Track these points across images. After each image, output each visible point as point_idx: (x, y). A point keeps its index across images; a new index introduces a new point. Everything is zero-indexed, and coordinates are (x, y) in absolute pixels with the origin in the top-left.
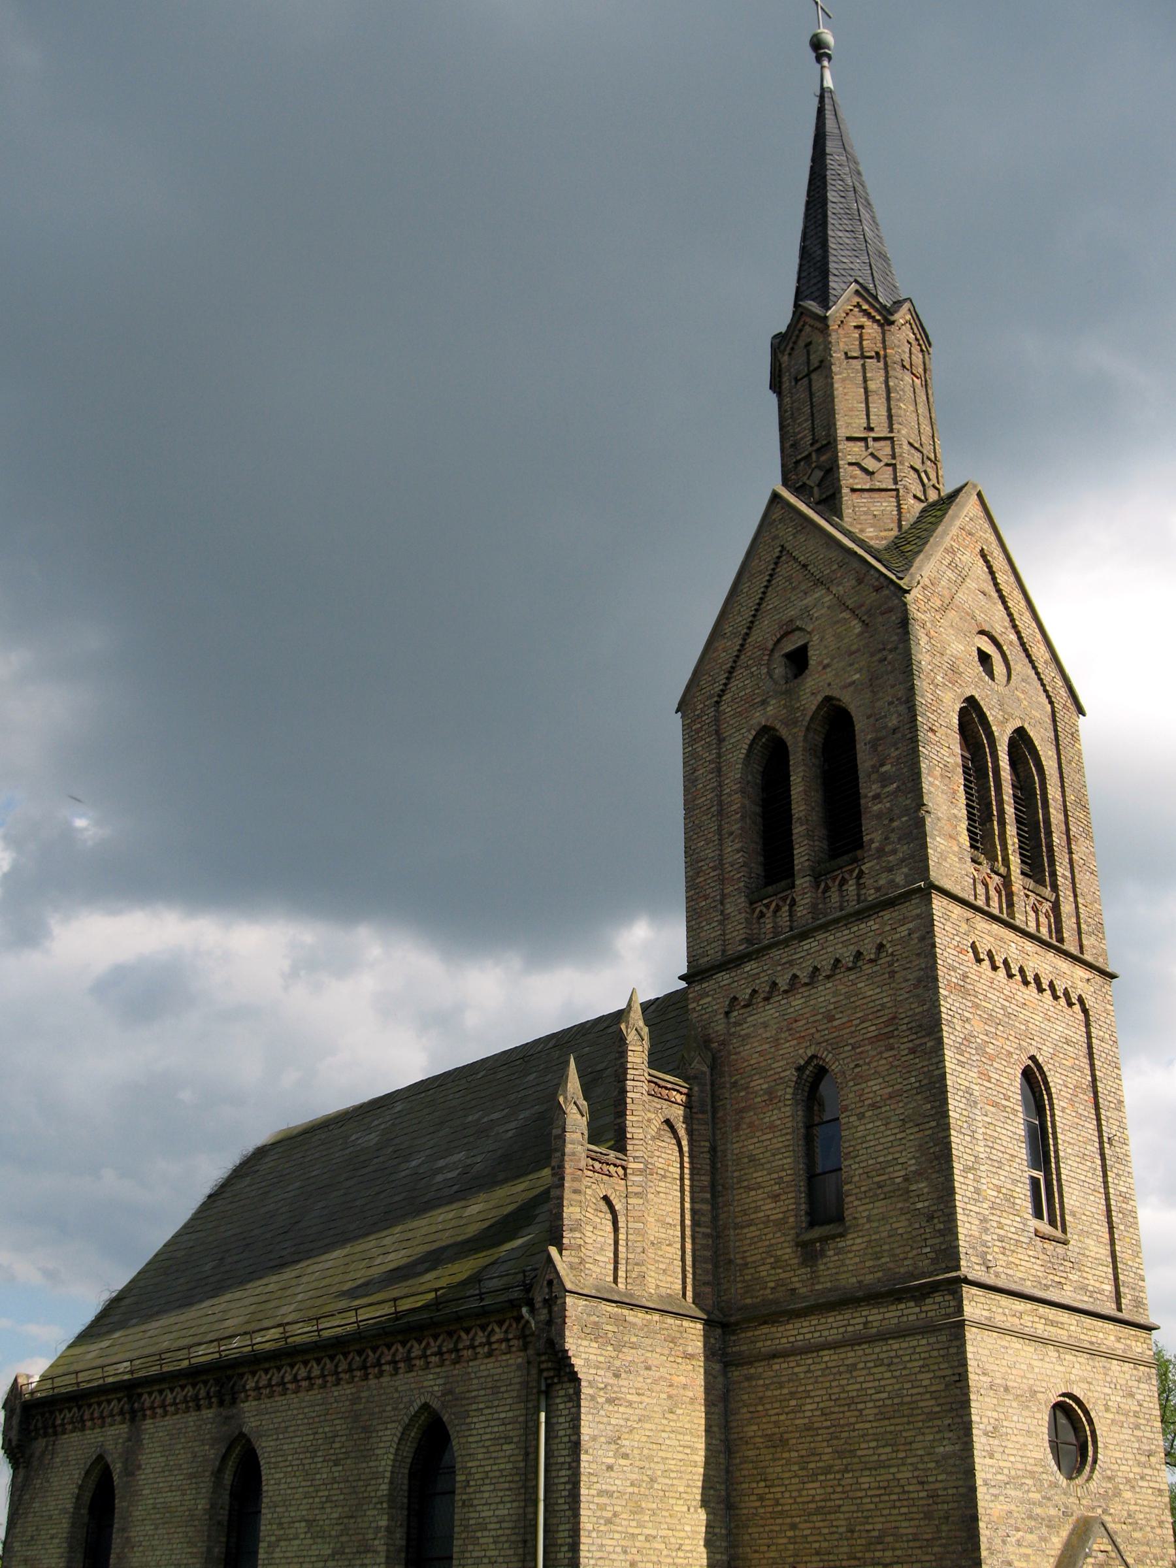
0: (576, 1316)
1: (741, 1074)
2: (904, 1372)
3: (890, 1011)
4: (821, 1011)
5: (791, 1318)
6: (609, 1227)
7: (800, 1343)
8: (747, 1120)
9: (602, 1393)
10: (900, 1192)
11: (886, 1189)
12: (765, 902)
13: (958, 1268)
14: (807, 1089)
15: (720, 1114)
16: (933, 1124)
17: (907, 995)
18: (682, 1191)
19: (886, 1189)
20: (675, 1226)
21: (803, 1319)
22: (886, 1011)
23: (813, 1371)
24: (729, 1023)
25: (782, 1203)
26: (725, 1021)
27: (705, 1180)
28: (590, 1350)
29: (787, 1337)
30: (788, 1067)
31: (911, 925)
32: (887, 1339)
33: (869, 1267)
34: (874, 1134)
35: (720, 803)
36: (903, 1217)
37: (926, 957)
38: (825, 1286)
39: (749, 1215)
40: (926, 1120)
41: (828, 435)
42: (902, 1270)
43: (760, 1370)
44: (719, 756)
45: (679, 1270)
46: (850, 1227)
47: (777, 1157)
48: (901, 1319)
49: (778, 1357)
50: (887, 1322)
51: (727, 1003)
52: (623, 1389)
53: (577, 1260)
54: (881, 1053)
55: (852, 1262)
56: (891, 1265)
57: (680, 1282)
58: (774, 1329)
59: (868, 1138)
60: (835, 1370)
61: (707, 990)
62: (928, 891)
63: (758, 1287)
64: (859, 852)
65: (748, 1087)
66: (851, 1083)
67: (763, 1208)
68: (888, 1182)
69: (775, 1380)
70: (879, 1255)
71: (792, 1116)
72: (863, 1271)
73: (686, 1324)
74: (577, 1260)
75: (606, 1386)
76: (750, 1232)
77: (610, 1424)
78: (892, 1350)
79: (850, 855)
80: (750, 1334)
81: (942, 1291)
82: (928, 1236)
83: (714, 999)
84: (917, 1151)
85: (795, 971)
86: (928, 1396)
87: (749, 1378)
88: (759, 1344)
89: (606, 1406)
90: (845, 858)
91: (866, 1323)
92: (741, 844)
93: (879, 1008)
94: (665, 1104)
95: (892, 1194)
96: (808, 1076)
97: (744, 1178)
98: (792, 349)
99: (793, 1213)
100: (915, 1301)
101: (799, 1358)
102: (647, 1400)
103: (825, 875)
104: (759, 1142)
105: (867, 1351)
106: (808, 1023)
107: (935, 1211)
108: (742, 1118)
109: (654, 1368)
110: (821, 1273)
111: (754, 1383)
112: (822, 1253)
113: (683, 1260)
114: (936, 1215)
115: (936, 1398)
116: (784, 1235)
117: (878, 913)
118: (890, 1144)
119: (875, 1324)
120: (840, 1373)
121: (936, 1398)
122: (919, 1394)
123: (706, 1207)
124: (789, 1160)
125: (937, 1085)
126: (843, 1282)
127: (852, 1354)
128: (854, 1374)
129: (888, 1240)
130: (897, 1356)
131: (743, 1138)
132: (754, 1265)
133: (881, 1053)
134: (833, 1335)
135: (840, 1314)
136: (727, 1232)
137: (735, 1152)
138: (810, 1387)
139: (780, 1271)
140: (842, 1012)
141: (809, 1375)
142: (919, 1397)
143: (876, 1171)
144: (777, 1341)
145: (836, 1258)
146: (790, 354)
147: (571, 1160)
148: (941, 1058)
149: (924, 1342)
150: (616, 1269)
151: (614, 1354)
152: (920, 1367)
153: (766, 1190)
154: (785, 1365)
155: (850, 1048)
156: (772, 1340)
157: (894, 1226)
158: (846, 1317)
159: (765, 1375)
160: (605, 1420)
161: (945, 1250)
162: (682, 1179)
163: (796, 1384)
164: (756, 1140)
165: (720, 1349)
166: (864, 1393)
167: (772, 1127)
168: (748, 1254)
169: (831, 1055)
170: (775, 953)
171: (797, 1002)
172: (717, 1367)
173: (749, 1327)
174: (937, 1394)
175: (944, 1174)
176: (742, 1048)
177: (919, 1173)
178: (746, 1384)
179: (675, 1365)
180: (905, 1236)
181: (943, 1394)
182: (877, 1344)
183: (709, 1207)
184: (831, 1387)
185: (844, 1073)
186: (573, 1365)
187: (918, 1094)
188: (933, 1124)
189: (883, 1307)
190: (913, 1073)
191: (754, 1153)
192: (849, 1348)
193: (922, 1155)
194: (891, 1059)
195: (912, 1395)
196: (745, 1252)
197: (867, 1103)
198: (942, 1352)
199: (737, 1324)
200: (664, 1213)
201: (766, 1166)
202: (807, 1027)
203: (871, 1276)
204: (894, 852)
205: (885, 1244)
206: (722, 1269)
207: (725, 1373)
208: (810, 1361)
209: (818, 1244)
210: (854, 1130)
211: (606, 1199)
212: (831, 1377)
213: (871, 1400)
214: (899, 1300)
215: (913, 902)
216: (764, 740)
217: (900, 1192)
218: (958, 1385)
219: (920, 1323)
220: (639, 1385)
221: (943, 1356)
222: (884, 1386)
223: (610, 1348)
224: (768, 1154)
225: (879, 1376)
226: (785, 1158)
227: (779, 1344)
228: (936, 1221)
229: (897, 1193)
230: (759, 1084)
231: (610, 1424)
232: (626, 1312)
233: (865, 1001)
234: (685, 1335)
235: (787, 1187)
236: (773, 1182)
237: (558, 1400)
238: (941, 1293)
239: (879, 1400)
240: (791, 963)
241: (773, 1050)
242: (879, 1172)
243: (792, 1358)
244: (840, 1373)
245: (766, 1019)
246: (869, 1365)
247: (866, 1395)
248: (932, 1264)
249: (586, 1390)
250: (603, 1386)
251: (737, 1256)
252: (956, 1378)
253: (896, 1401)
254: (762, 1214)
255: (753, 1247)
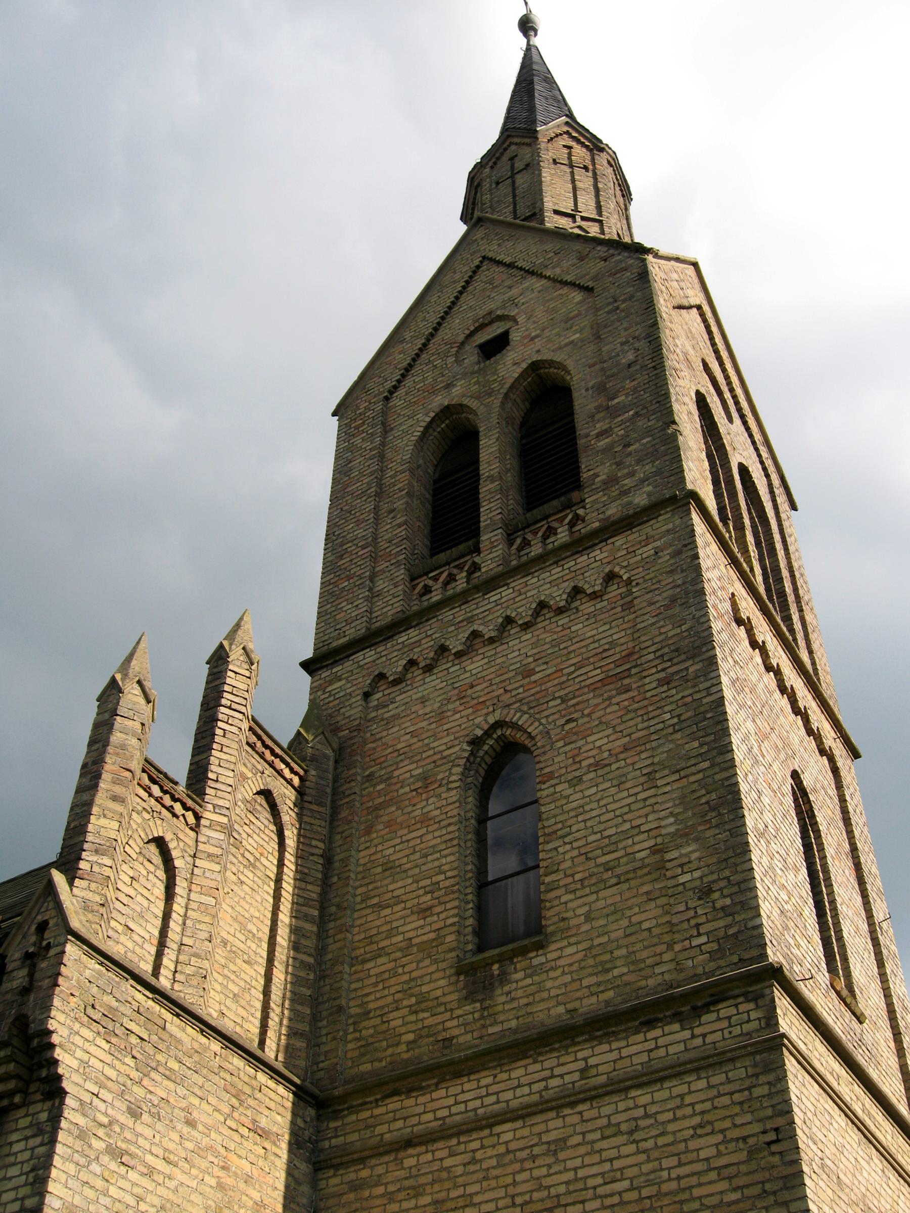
0: (78, 981)
1: (380, 764)
2: (661, 1141)
3: (624, 647)
4: (512, 668)
5: (444, 1080)
6: (159, 890)
7: (458, 1118)
8: (385, 819)
9: (101, 1132)
10: (646, 871)
11: (618, 871)
12: (431, 575)
13: (765, 956)
14: (482, 773)
15: (344, 814)
16: (706, 764)
17: (653, 620)
18: (277, 896)
19: (618, 871)
20: (260, 940)
21: (465, 1079)
22: (618, 649)
23: (481, 1161)
24: (367, 708)
25: (435, 918)
26: (363, 703)
27: (314, 891)
28: (93, 1049)
29: (434, 1111)
30: (457, 742)
31: (658, 543)
32: (627, 1089)
33: (588, 987)
34: (598, 801)
35: (380, 485)
36: (652, 904)
37: (683, 571)
38: (506, 1026)
39: (377, 942)
40: (692, 762)
41: (533, 205)
42: (651, 982)
43: (380, 1170)
44: (383, 444)
45: (259, 1005)
46: (553, 934)
47: (430, 858)
48: (653, 1055)
49: (415, 1145)
50: (627, 1062)
51: (369, 681)
52: (141, 1141)
53: (97, 898)
54: (610, 698)
55: (557, 983)
56: (631, 978)
57: (257, 1023)
58: (411, 1102)
59: (587, 808)
60: (524, 1154)
61: (339, 674)
62: (684, 502)
63: (385, 1043)
64: (575, 496)
65: (389, 778)
66: (561, 744)
67: (401, 929)
68: (624, 860)
69: (407, 1183)
70: (608, 966)
71: (459, 801)
72: (579, 994)
73: (262, 1077)
74: (97, 898)
75: (111, 1123)
76: (383, 964)
77: (106, 1193)
78: (637, 1107)
79: (562, 499)
80: (365, 1114)
81: (735, 997)
82: (703, 919)
83: (348, 682)
84: (675, 806)
85: (475, 627)
86: (713, 1175)
87: (355, 1187)
88: (379, 1130)
89: (105, 1159)
90: (555, 503)
91: (583, 1071)
92: (404, 518)
93: (606, 647)
94: (269, 771)
95: (631, 875)
96: (486, 753)
97: (373, 893)
98: (495, 163)
99: (454, 929)
100: (681, 1022)
101: (454, 1141)
102: (181, 1177)
103: (523, 529)
104: (402, 842)
105: (587, 1115)
106: (491, 685)
107: (714, 881)
108: (377, 817)
109: (200, 1127)
110: (500, 1008)
111: (366, 1193)
112: (503, 978)
113: (267, 992)
114: (715, 887)
115: (730, 1178)
116: (436, 962)
117: (606, 540)
118: (626, 809)
119: (601, 1069)
120: (534, 1158)
121: (730, 1178)
122: (693, 1174)
123: (312, 928)
124: (451, 858)
125: (709, 715)
126: (542, 1016)
127: (559, 1122)
128: (562, 1155)
129: (624, 942)
130: (646, 1116)
131: (376, 842)
132: (378, 1013)
133: (610, 698)
134: (524, 1096)
135: (535, 1062)
136: (339, 968)
137: (362, 861)
138: (470, 1189)
139: (426, 1015)
140: (547, 663)
141: (472, 1168)
142: (694, 1180)
143: (602, 848)
144: (415, 1120)
145: (529, 981)
146: (492, 167)
147: (117, 754)
148: (715, 681)
149: (702, 1084)
150: (159, 955)
151: (135, 1075)
152: (694, 1128)
153: (409, 904)
154: (429, 1157)
155: (559, 701)
156: (405, 1118)
157: (634, 919)
158: (547, 1064)
159: (390, 1177)
160: (99, 1183)
161: (735, 935)
162: (278, 880)
163: (447, 1185)
164: (398, 841)
165: (309, 1141)
166: (580, 1185)
167: (425, 820)
168: (372, 997)
169: (527, 716)
170: (447, 615)
171: (475, 665)
172: (304, 1167)
173: (365, 1103)
174: (732, 1170)
175: (727, 827)
176: (385, 733)
177: (683, 835)
178: (352, 1196)
179: (236, 1137)
180: (655, 931)
181: (743, 1168)
182: (607, 1099)
183: (315, 929)
184: (515, 1183)
185: (548, 733)
186: (56, 1062)
187: (675, 732)
188: (706, 764)
189: (618, 1040)
190: (667, 709)
191: (392, 858)
192: (553, 1114)
193: (686, 810)
194: (626, 703)
195: (679, 1178)
196: (367, 995)
197: (584, 763)
198: (737, 1097)
199: (344, 1098)
200: (247, 915)
201: (410, 873)
202: (490, 689)
203: (594, 999)
204: (632, 474)
205: (618, 947)
206: (325, 1023)
207: (314, 1184)
208: (476, 1145)
209: (496, 966)
210: (564, 802)
211: (160, 843)
212: (517, 1166)
213: (596, 1197)
214: (650, 1024)
215: (660, 518)
216: (443, 426)
217: (646, 871)
218: (774, 1148)
219: (692, 1055)
220: (171, 1146)
221: (741, 1103)
222: (621, 1169)
223: (129, 1060)
224: (417, 855)
225: (613, 1153)
226: (445, 856)
227: (419, 1124)
228: (716, 895)
229: (640, 873)
230: (408, 771)
231: (106, 1193)
232: (168, 1016)
233: (583, 644)
234: (258, 1095)
235: (446, 894)
236: (421, 892)
237: (14, 1137)
238: (732, 1002)
239: (612, 1195)
240: (470, 620)
241: (433, 726)
242: (606, 850)
243: (440, 1144)
244: (534, 1158)
245: (425, 693)
246: (590, 1137)
247: (586, 1189)
248: (711, 959)
249: (71, 1116)
250: (105, 1120)
251: (352, 1003)
252: (772, 1136)
253: (645, 1192)
254: (400, 938)
255: (381, 986)
